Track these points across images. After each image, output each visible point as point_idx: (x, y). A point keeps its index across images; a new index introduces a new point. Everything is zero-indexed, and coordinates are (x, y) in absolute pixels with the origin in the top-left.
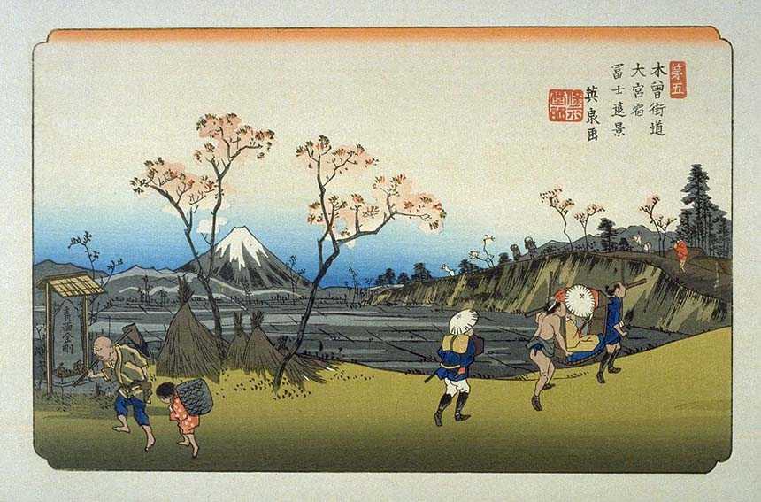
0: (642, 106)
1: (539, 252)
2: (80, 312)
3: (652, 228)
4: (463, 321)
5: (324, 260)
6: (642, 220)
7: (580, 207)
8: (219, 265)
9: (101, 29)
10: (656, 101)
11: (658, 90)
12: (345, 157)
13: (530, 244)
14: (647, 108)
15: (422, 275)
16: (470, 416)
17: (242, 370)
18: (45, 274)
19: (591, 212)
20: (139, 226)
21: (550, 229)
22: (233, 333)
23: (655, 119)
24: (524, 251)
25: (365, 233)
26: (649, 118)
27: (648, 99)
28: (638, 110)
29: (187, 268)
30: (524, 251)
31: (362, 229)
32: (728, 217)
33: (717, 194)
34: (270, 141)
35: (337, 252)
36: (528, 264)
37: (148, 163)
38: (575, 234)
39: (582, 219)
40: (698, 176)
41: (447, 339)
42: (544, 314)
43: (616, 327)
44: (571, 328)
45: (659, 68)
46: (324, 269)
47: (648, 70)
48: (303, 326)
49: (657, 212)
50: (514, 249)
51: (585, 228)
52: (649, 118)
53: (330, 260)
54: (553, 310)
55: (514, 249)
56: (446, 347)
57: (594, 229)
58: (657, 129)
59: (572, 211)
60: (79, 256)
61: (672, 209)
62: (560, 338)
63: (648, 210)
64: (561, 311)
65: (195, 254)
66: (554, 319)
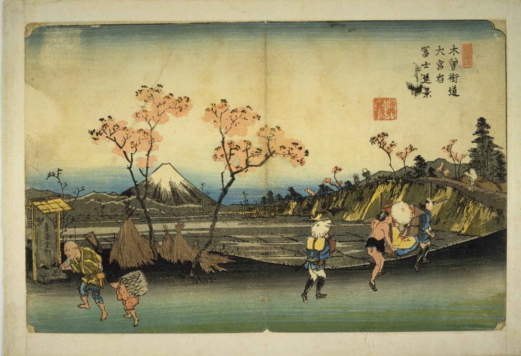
0: (443, 76)
1: (373, 178)
2: (55, 224)
3: (450, 160)
4: (321, 228)
5: (225, 184)
6: (445, 155)
7: (400, 148)
8: (151, 191)
9: (70, 26)
10: (453, 72)
11: (454, 64)
12: (238, 114)
13: (366, 174)
14: (446, 77)
15: (293, 194)
16: (482, 122)
17: (372, 173)
18: (35, 197)
19: (408, 151)
20: (98, 164)
21: (378, 163)
22: (163, 233)
23: (452, 84)
24: (362, 178)
25: (252, 166)
26: (448, 84)
27: (447, 72)
28: (440, 78)
29: (128, 193)
30: (362, 178)
31: (250, 164)
32: (503, 151)
33: (495, 133)
34: (187, 104)
35: (233, 179)
36: (358, 190)
37: (102, 120)
38: (398, 165)
39: (403, 157)
40: (482, 122)
41: (310, 240)
42: (377, 221)
43: (427, 231)
44: (396, 231)
45: (454, 49)
46: (225, 191)
47: (447, 50)
48: (212, 228)
49: (454, 149)
50: (356, 177)
51: (404, 162)
52: (448, 84)
53: (229, 184)
54: (384, 219)
55: (356, 177)
56: (310, 246)
57: (411, 162)
58: (453, 92)
59: (395, 150)
60: (52, 185)
61: (464, 148)
62: (388, 239)
63: (448, 149)
64: (388, 220)
65: (135, 182)
66: (385, 226)
